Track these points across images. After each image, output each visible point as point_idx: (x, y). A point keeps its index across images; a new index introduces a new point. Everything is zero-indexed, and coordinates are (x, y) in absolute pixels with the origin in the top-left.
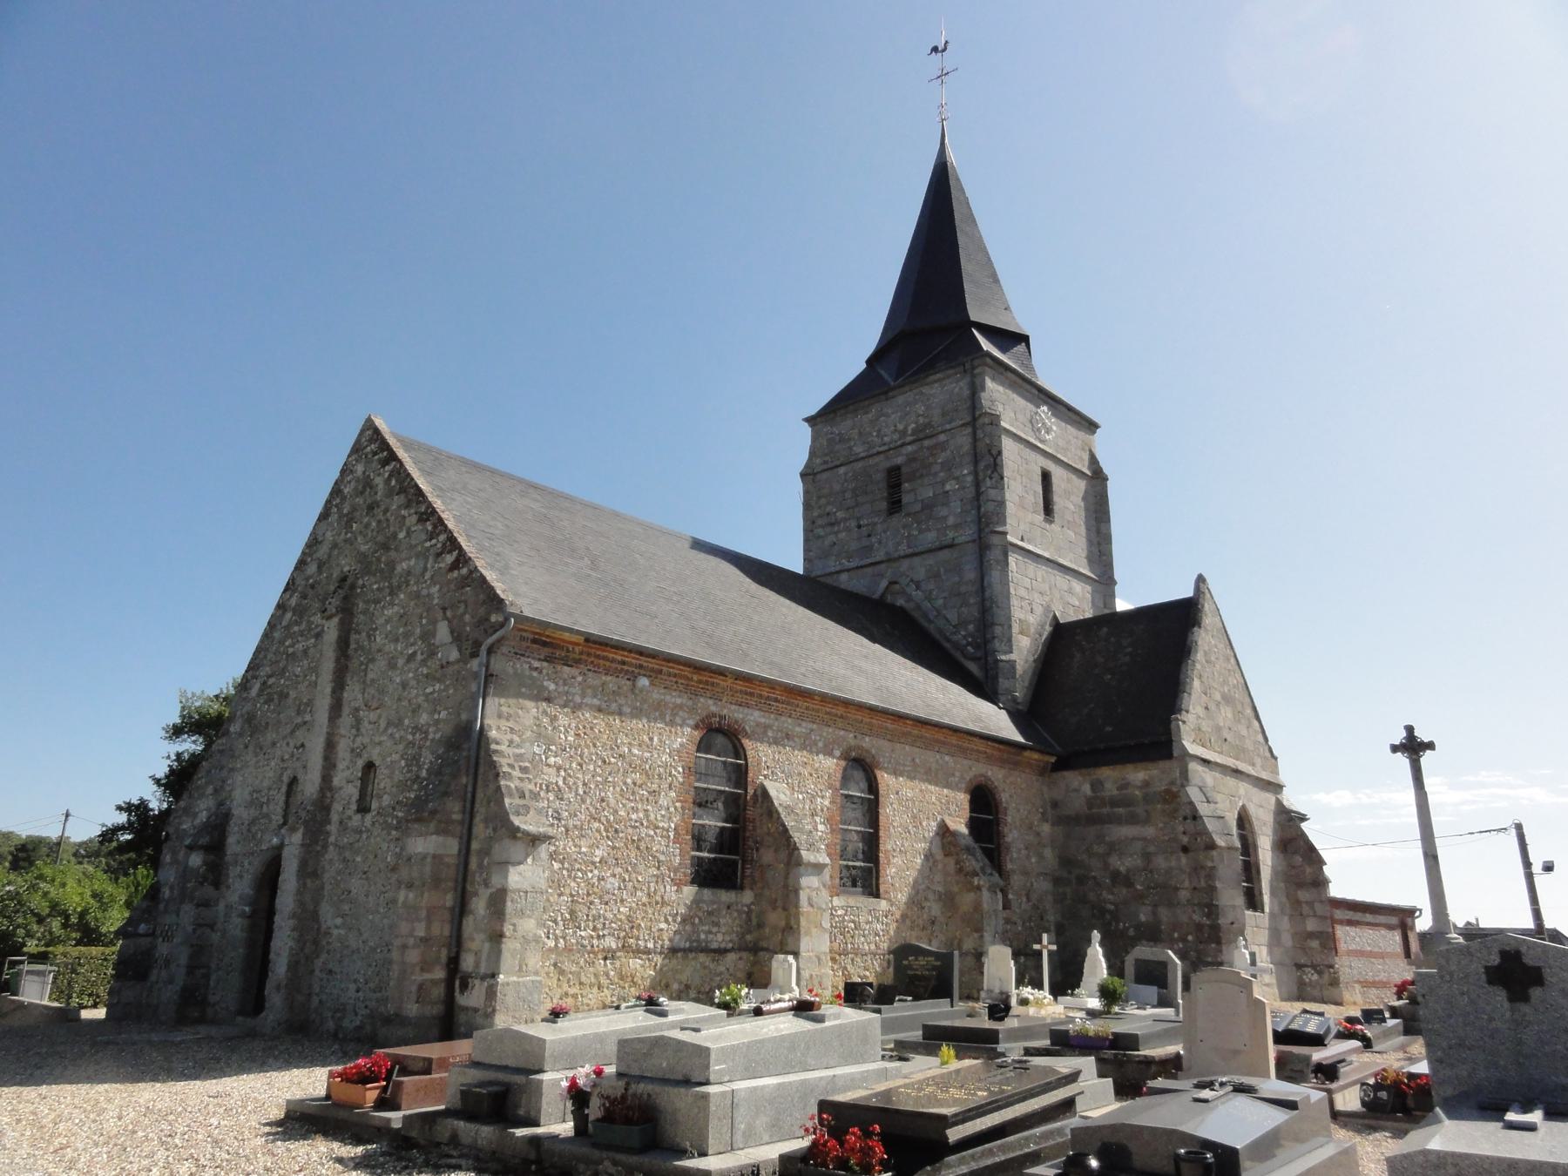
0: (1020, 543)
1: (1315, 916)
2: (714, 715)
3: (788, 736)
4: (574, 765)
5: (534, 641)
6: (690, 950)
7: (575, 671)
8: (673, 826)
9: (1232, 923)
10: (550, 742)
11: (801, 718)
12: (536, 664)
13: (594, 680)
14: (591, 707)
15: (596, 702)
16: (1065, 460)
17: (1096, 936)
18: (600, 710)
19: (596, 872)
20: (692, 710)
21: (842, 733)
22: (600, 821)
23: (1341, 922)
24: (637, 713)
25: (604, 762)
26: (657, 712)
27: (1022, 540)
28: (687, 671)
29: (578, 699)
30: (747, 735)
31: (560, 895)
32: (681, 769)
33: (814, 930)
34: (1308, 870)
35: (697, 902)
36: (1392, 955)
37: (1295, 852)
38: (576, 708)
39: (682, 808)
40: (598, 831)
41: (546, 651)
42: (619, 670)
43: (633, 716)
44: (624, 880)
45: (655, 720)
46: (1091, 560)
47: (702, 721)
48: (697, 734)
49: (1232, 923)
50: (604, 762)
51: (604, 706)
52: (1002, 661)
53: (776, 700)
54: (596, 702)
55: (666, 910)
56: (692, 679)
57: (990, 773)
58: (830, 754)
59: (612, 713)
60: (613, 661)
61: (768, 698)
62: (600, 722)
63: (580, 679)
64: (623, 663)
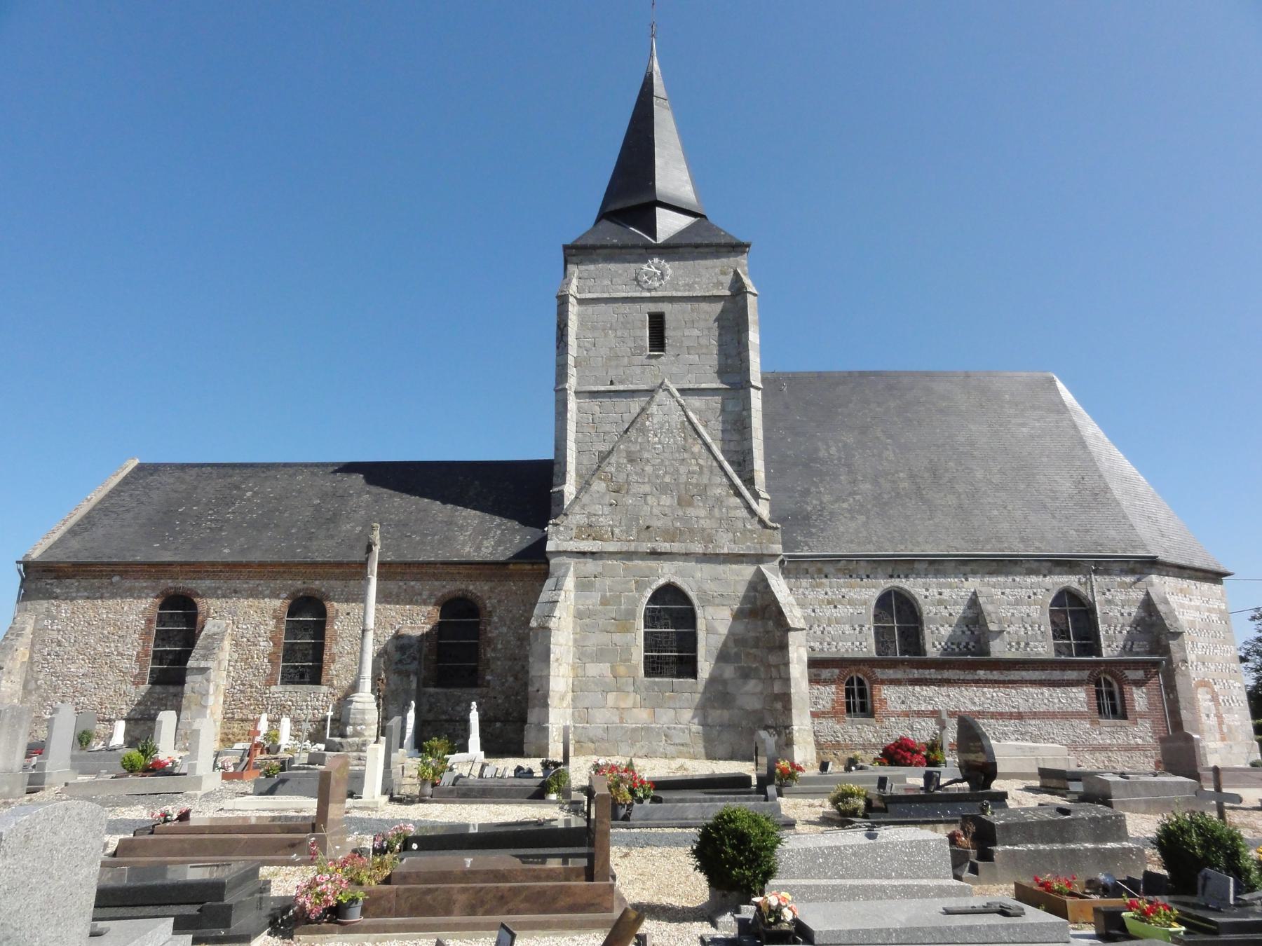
0: (612, 388)
1: (780, 678)
2: (171, 588)
3: (235, 592)
4: (69, 628)
5: (44, 571)
6: (140, 720)
7: (73, 581)
8: (135, 653)
9: (538, 691)
10: (54, 618)
11: (249, 578)
12: (49, 581)
13: (84, 583)
14: (81, 598)
15: (86, 594)
16: (680, 294)
17: (474, 704)
18: (88, 598)
19: (79, 680)
20: (153, 589)
21: (290, 582)
22: (84, 655)
23: (882, 682)
24: (113, 596)
25: (89, 624)
26: (131, 593)
27: (612, 383)
28: (146, 568)
29: (74, 595)
30: (198, 595)
31: (56, 693)
32: (143, 622)
33: (193, 707)
34: (778, 634)
35: (149, 693)
36: (1079, 715)
37: (770, 619)
38: (72, 599)
39: (144, 643)
40: (83, 659)
41: (54, 574)
42: (100, 575)
43: (110, 598)
44: (98, 684)
45: (126, 597)
46: (722, 373)
47: (162, 593)
48: (158, 601)
49: (538, 691)
50: (89, 624)
51: (91, 595)
52: (554, 492)
53: (221, 571)
54: (86, 594)
55: (127, 699)
56: (151, 571)
57: (471, 587)
58: (277, 597)
59: (97, 598)
60: (94, 571)
61: (214, 571)
62: (88, 604)
63: (76, 584)
64: (101, 571)
